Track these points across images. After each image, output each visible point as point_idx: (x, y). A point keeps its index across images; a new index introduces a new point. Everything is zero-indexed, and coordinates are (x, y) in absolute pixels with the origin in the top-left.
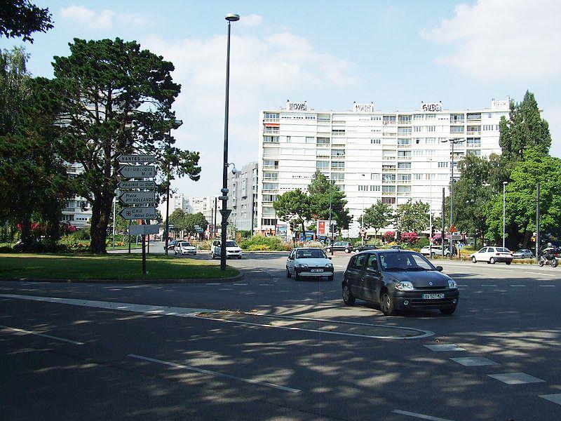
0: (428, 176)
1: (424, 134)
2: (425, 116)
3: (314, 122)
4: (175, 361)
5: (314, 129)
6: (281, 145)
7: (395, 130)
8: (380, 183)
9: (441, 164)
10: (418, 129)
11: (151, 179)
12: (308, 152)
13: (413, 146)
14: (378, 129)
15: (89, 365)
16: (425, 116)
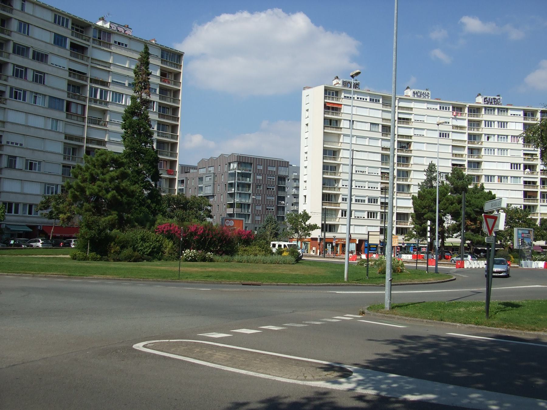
0: (500, 178)
1: (495, 130)
2: (496, 110)
3: (379, 106)
4: (261, 371)
5: (379, 114)
6: (344, 131)
7: (465, 123)
8: (521, 161)
9: (514, 166)
10: (489, 123)
11: (123, 194)
12: (373, 143)
13: (485, 144)
14: (447, 120)
15: (432, 358)
16: (496, 110)
